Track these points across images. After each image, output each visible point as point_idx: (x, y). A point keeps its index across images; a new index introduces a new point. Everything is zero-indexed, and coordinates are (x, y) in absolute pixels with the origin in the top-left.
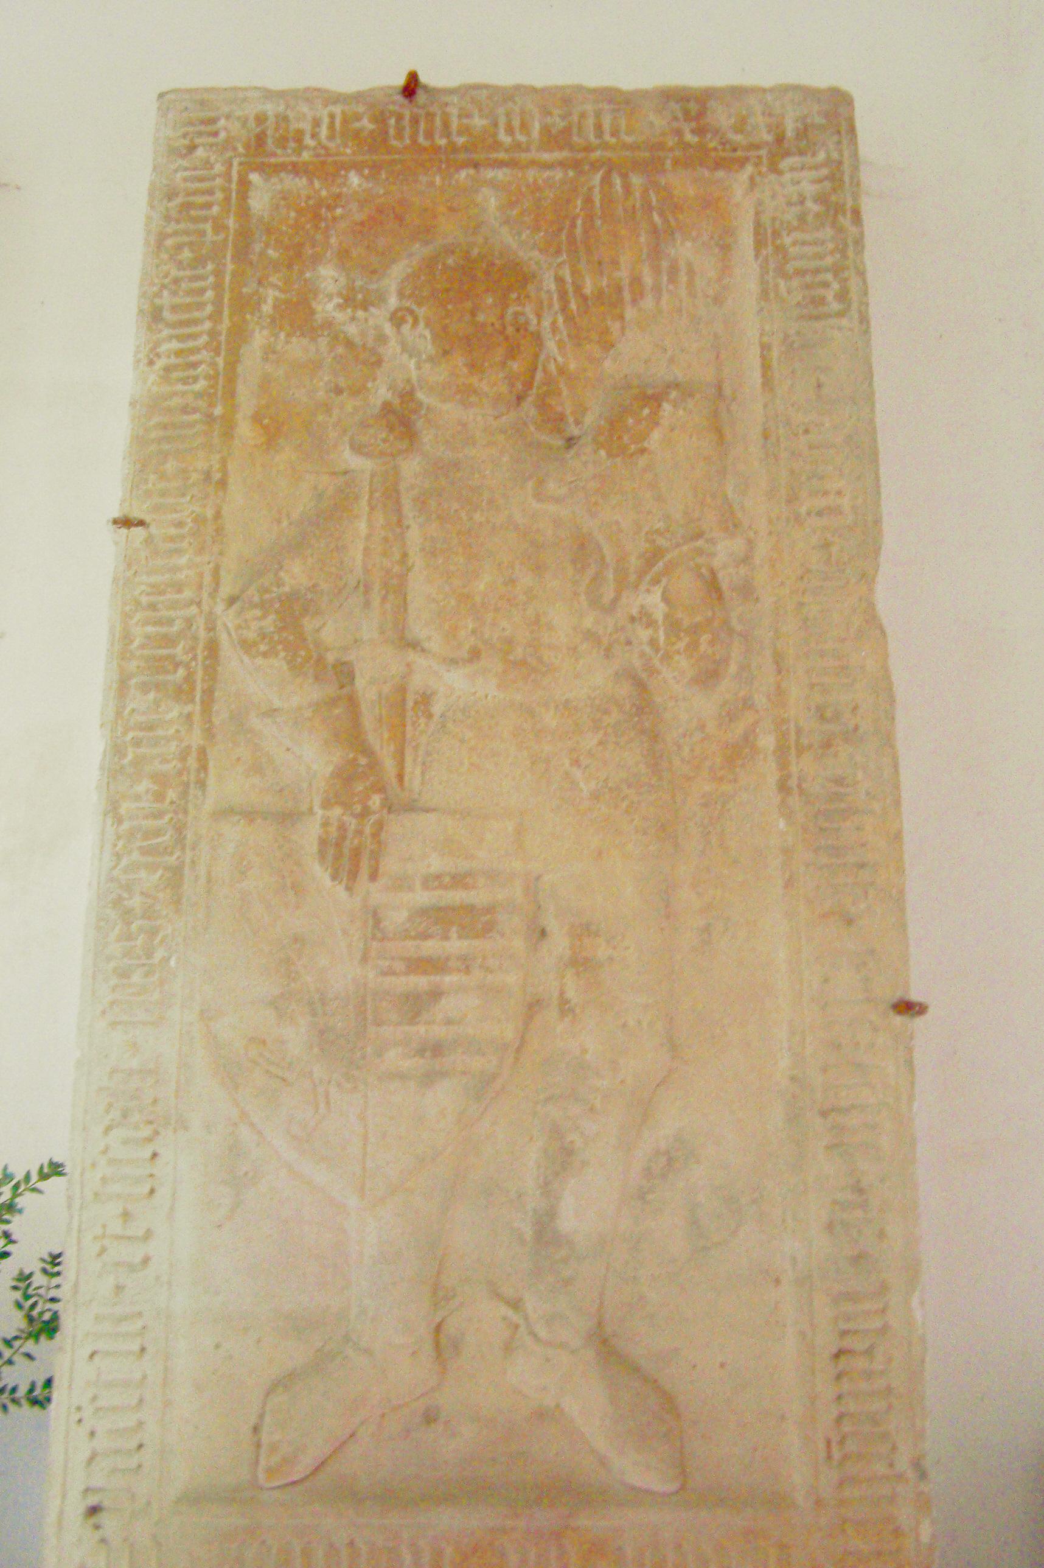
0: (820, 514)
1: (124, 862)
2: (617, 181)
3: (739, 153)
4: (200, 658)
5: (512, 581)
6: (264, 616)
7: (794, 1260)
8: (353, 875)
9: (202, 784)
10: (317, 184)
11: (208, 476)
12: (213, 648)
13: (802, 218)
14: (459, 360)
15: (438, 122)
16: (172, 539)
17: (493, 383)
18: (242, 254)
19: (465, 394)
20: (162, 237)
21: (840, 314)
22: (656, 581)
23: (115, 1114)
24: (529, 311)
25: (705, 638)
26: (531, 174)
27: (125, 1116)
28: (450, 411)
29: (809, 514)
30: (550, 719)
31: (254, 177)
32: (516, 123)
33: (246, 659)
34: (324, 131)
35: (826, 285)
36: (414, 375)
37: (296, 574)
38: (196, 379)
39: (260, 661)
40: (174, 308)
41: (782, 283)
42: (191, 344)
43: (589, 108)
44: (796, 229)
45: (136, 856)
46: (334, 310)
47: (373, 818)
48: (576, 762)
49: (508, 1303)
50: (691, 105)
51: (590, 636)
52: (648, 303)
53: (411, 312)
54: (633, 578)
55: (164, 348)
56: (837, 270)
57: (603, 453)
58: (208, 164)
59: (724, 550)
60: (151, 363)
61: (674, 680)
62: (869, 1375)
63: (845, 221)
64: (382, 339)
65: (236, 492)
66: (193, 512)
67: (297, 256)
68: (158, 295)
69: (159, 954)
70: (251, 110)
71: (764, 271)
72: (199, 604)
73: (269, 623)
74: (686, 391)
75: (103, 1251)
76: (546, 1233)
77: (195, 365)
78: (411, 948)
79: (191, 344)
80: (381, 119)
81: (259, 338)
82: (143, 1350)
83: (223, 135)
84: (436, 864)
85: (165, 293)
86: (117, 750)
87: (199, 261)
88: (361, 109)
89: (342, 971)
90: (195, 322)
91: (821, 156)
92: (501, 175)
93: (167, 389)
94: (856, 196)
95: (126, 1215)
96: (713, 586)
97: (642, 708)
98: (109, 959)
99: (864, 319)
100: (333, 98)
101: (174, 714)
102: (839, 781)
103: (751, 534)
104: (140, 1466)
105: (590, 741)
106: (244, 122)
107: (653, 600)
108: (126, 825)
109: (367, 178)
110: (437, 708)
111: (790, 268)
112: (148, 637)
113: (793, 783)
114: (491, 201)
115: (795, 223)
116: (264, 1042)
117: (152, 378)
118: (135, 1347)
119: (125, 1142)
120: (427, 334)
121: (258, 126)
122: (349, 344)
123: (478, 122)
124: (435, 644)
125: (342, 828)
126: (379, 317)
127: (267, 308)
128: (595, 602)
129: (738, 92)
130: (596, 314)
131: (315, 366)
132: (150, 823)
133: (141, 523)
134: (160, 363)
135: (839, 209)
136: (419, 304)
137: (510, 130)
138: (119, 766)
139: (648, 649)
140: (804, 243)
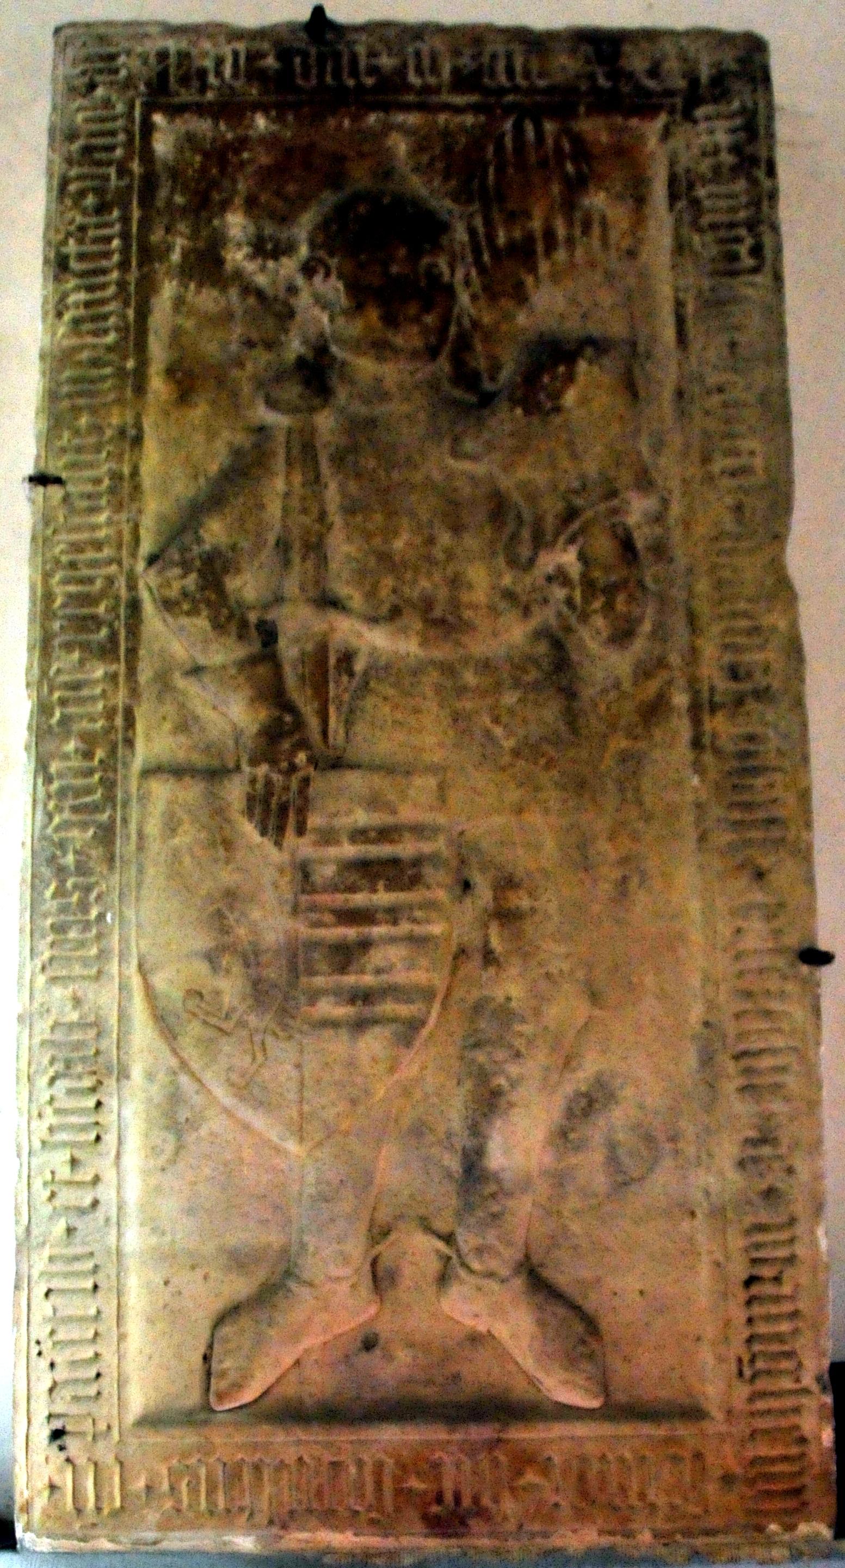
0: (733, 474)
1: (57, 820)
2: (529, 129)
3: (654, 100)
4: (122, 617)
5: (431, 541)
6: (184, 576)
7: (707, 1193)
8: (281, 830)
9: (130, 743)
10: (223, 126)
11: (122, 432)
12: (135, 606)
13: (717, 169)
14: (373, 314)
15: (345, 60)
16: (89, 496)
17: (408, 338)
18: (147, 199)
19: (380, 348)
20: (64, 183)
21: (756, 270)
22: (572, 540)
23: (59, 1066)
24: (443, 263)
25: (621, 599)
26: (442, 118)
27: (68, 1067)
28: (365, 366)
29: (723, 472)
30: (470, 678)
31: (158, 118)
32: (426, 63)
33: (170, 620)
34: (228, 71)
35: (738, 240)
36: (328, 330)
37: (215, 531)
38: (106, 332)
39: (185, 621)
40: (82, 257)
41: (696, 239)
42: (98, 295)
43: (500, 49)
44: (711, 181)
45: (67, 815)
46: (245, 258)
47: (301, 774)
48: (496, 720)
49: (440, 1237)
50: (603, 45)
51: (509, 595)
52: (561, 255)
53: (321, 261)
54: (549, 538)
55: (72, 299)
56: (752, 225)
57: (519, 411)
58: (107, 103)
59: (637, 509)
60: (59, 315)
61: (591, 639)
62: (777, 1299)
63: (761, 174)
64: (292, 290)
65: (151, 445)
66: (110, 470)
67: (204, 203)
68: (64, 243)
69: (94, 913)
70: (151, 47)
71: (678, 223)
72: (120, 563)
73: (191, 581)
74: (597, 346)
75: (53, 1195)
76: (473, 1170)
77: (105, 317)
78: (340, 899)
79: (98, 295)
80: (284, 54)
81: (168, 289)
82: (96, 1287)
83: (123, 73)
84: (361, 817)
85: (71, 241)
86: (43, 709)
87: (101, 209)
88: (266, 46)
89: (271, 922)
90: (104, 272)
91: (736, 105)
92: (412, 119)
93: (74, 341)
94: (771, 148)
95: (74, 1162)
96: (627, 545)
97: (557, 666)
98: (45, 916)
99: (778, 278)
100: (236, 34)
101: (99, 673)
102: (751, 738)
103: (665, 494)
104: (99, 1393)
105: (510, 698)
106: (145, 59)
107: (569, 558)
108: (55, 786)
109: (273, 121)
110: (359, 666)
111: (705, 220)
112: (70, 596)
113: (706, 740)
114: (400, 146)
115: (710, 175)
116: (201, 995)
117: (61, 330)
118: (89, 1284)
119: (70, 1092)
120: (340, 286)
121: (159, 62)
122: (260, 294)
123: (386, 62)
124: (357, 600)
125: (268, 783)
126: (288, 267)
127: (176, 257)
128: (513, 562)
129: (650, 35)
130: (509, 267)
131: (227, 317)
132: (79, 782)
133: (58, 481)
134: (67, 317)
135: (754, 161)
136: (331, 254)
137: (419, 71)
138: (45, 731)
139: (565, 609)
140: (718, 196)
